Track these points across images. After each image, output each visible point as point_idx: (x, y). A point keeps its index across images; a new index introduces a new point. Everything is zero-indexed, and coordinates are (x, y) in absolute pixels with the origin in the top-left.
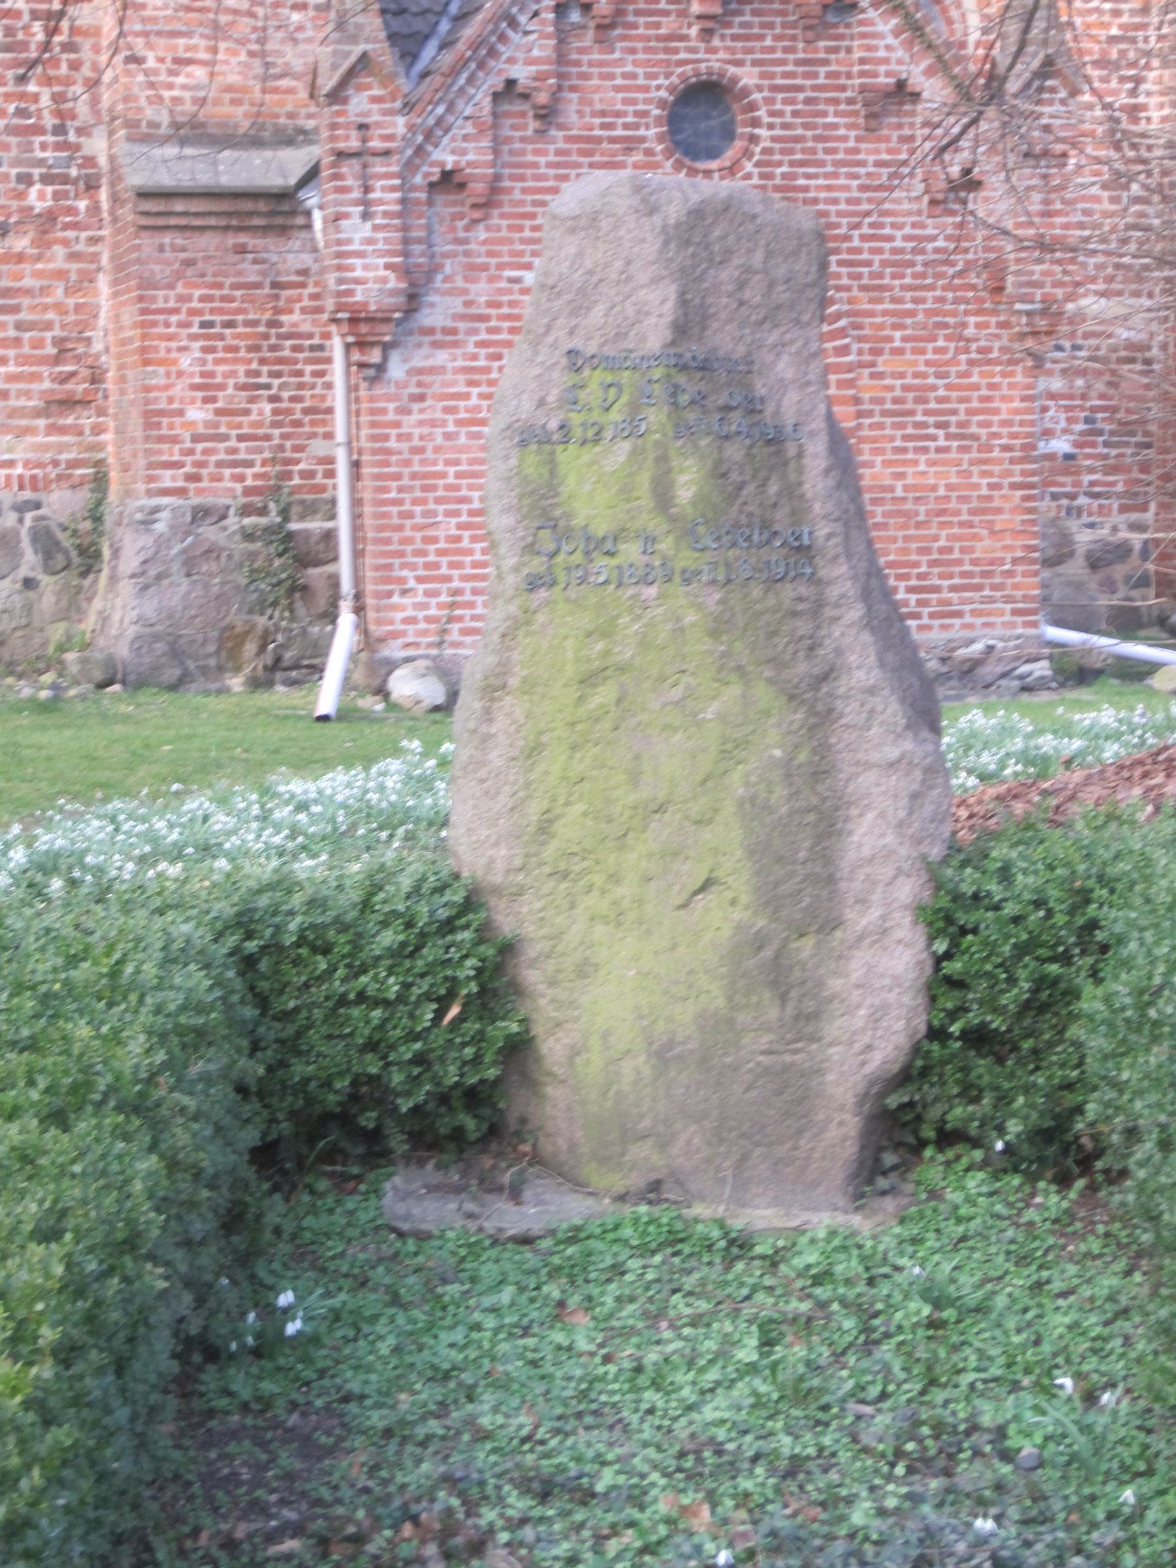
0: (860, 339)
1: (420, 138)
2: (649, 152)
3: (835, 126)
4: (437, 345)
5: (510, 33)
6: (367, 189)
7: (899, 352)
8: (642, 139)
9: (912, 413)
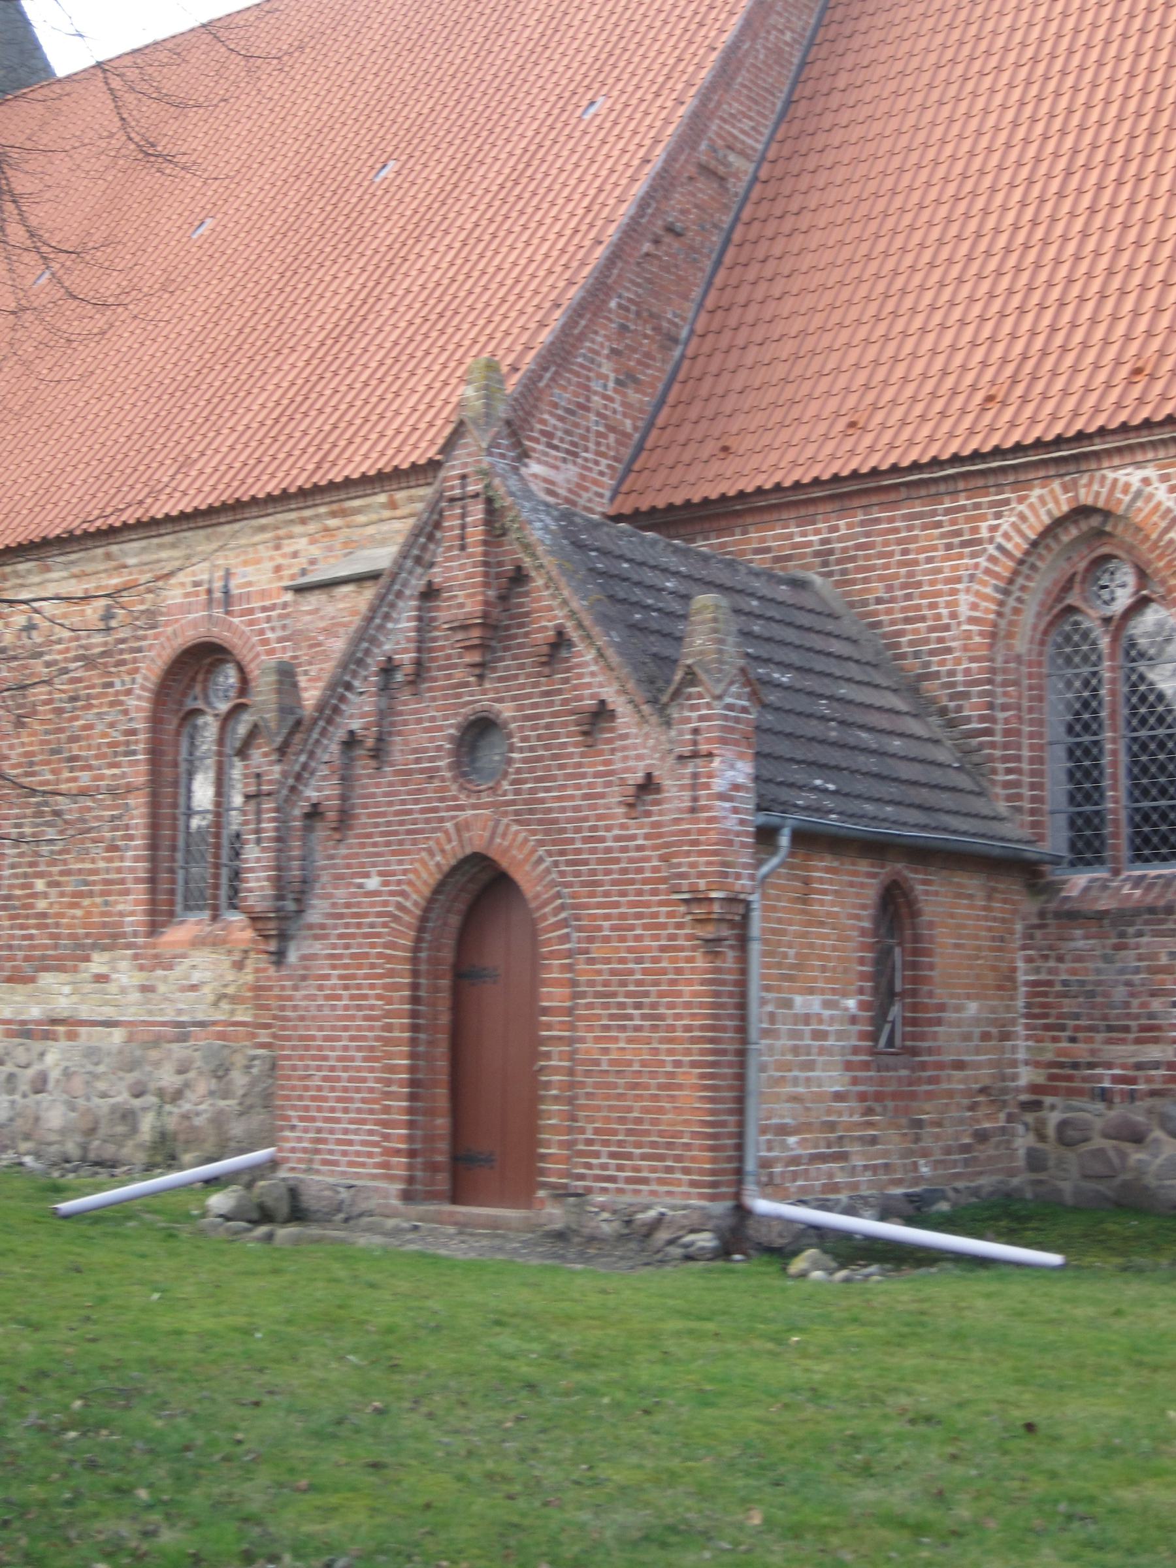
0: (580, 929)
1: (291, 781)
2: (443, 779)
3: (564, 745)
4: (317, 937)
5: (348, 695)
6: (259, 821)
7: (607, 939)
8: (438, 769)
9: (614, 995)
